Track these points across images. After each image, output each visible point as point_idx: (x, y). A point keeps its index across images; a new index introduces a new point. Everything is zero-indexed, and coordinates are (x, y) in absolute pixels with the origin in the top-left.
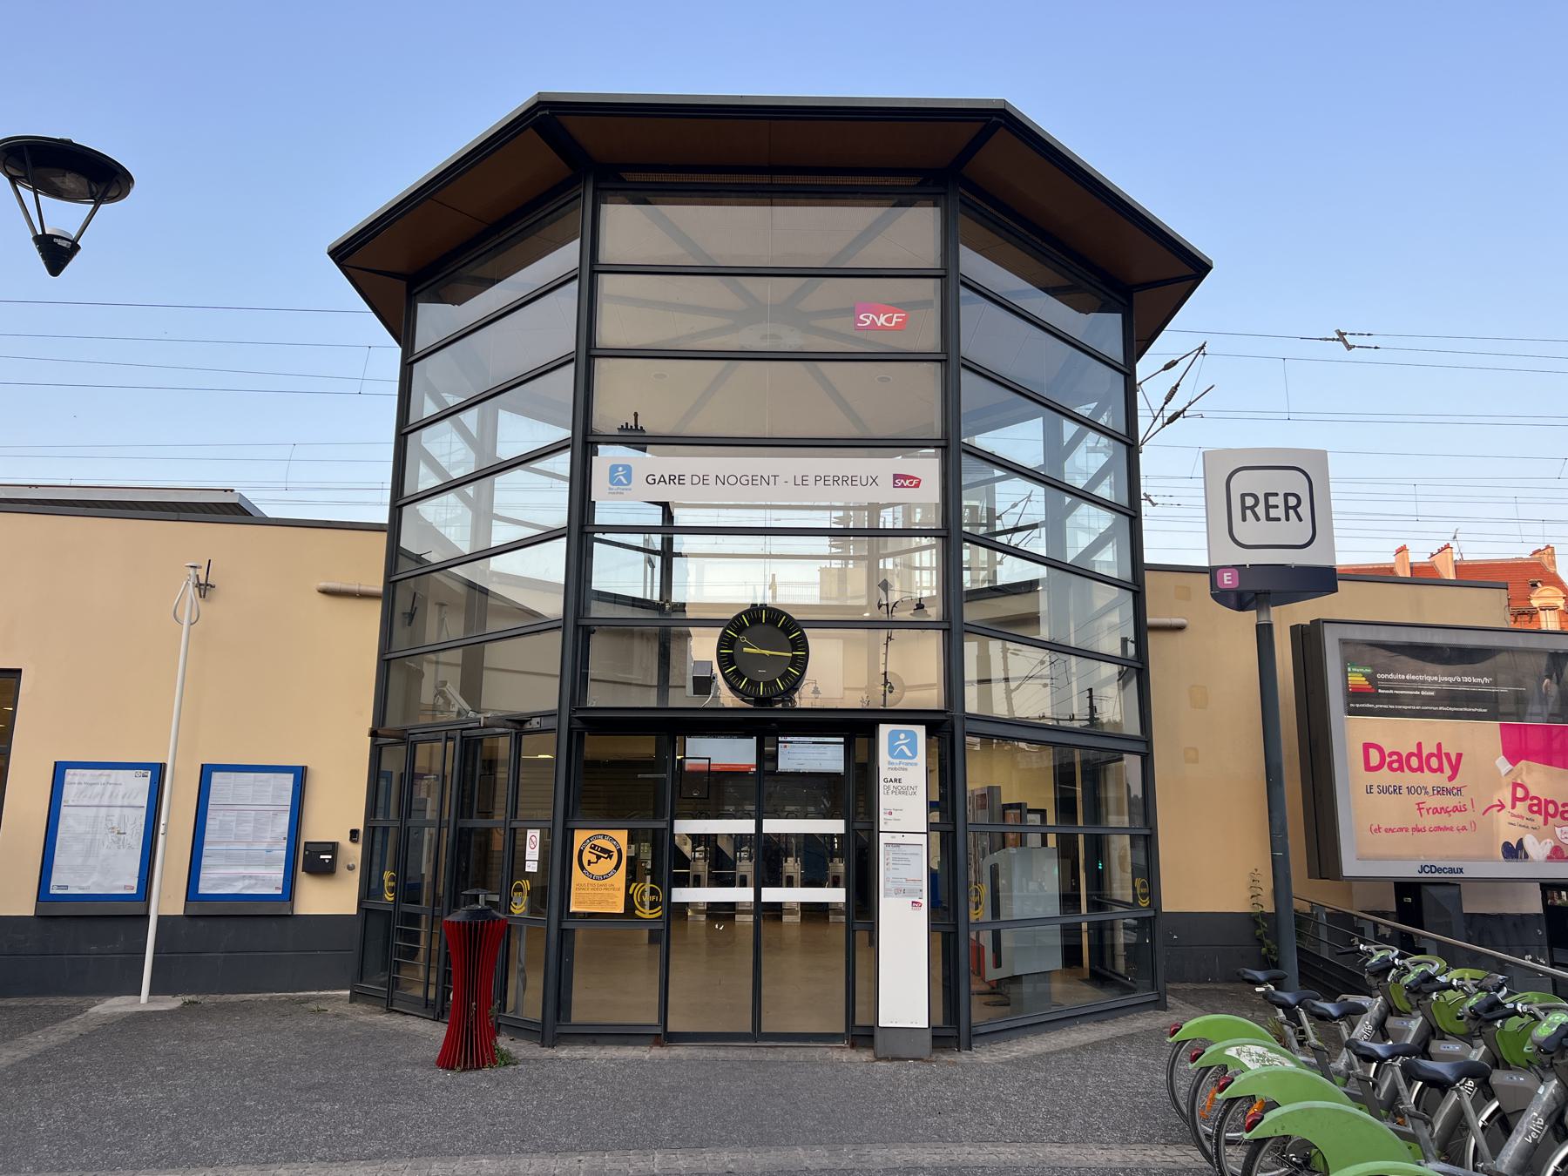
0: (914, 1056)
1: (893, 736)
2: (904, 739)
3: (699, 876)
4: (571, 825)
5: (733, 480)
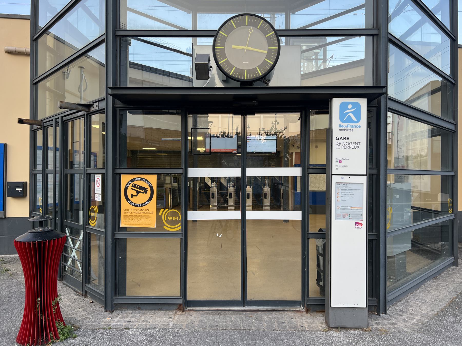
0: (356, 326)
1: (343, 107)
2: (351, 109)
3: (214, 193)
4: (118, 171)
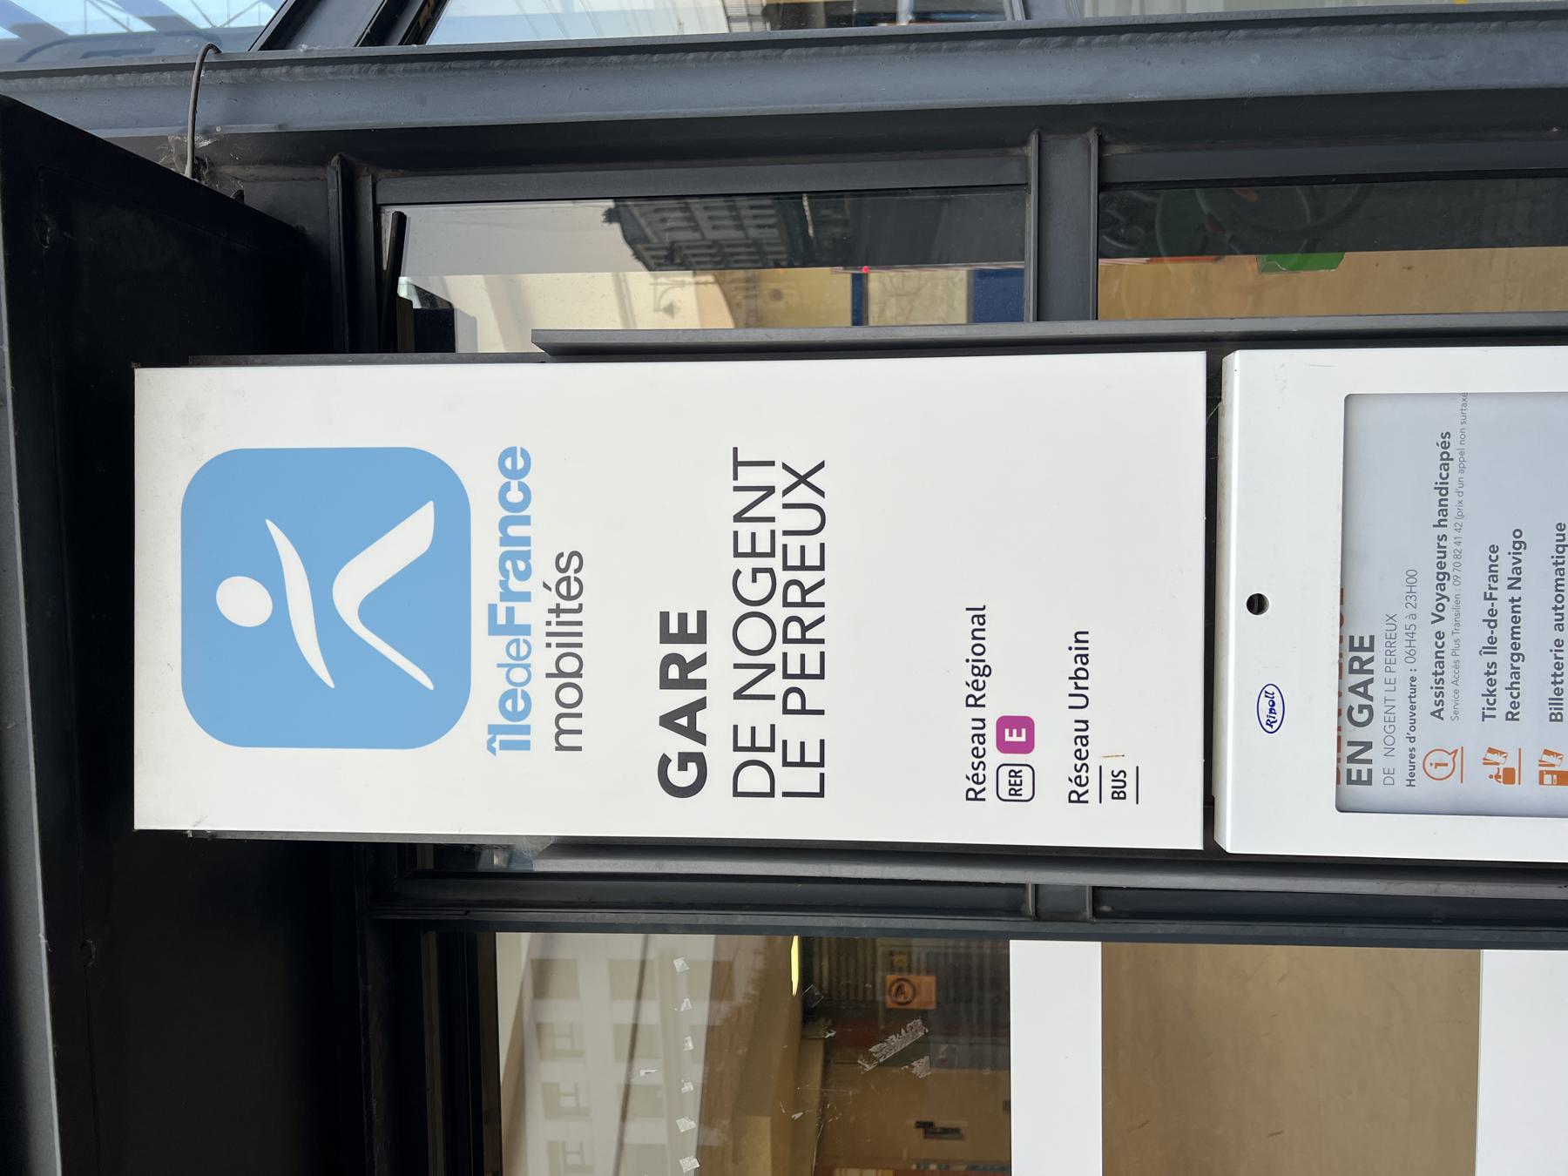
5: (1389, 740)
